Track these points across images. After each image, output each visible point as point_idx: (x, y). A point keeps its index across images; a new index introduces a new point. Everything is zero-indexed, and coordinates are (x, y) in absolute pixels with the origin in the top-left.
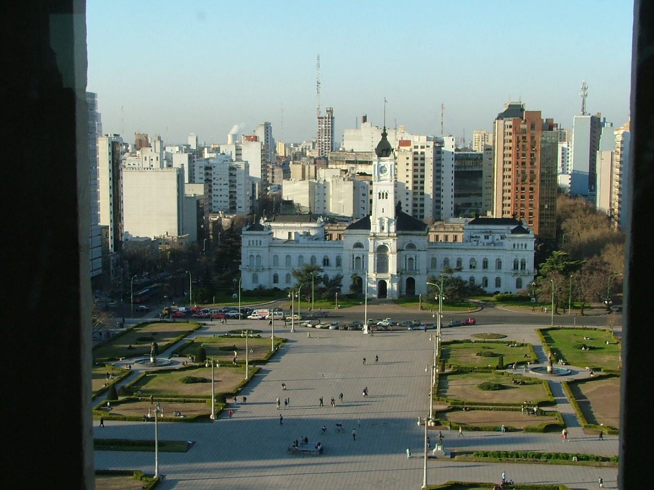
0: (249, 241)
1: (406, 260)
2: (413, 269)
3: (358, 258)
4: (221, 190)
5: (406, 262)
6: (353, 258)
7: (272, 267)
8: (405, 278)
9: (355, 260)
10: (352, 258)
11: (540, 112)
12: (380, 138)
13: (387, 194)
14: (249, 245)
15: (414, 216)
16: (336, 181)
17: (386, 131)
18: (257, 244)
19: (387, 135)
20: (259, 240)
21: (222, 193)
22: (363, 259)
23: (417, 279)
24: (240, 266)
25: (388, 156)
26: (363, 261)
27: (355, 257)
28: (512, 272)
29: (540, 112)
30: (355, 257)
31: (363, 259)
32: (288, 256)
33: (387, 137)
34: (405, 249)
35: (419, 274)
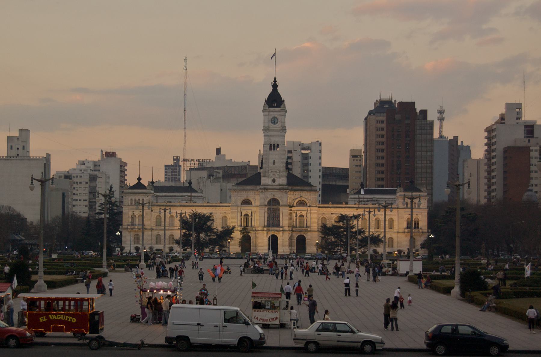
0: (131, 199)
1: (296, 217)
2: (304, 225)
3: (246, 215)
4: (81, 177)
5: (296, 219)
6: (241, 216)
7: (154, 228)
8: (296, 235)
9: (243, 217)
10: (239, 215)
11: (426, 110)
12: (270, 89)
13: (278, 145)
14: (131, 204)
15: (304, 177)
16: (203, 183)
17: (279, 89)
19: (277, 86)
21: (81, 180)
22: (252, 216)
23: (308, 236)
24: (121, 227)
26: (251, 219)
27: (243, 214)
28: (406, 230)
29: (426, 110)
30: (243, 214)
33: (278, 88)
34: (295, 205)
35: (310, 231)
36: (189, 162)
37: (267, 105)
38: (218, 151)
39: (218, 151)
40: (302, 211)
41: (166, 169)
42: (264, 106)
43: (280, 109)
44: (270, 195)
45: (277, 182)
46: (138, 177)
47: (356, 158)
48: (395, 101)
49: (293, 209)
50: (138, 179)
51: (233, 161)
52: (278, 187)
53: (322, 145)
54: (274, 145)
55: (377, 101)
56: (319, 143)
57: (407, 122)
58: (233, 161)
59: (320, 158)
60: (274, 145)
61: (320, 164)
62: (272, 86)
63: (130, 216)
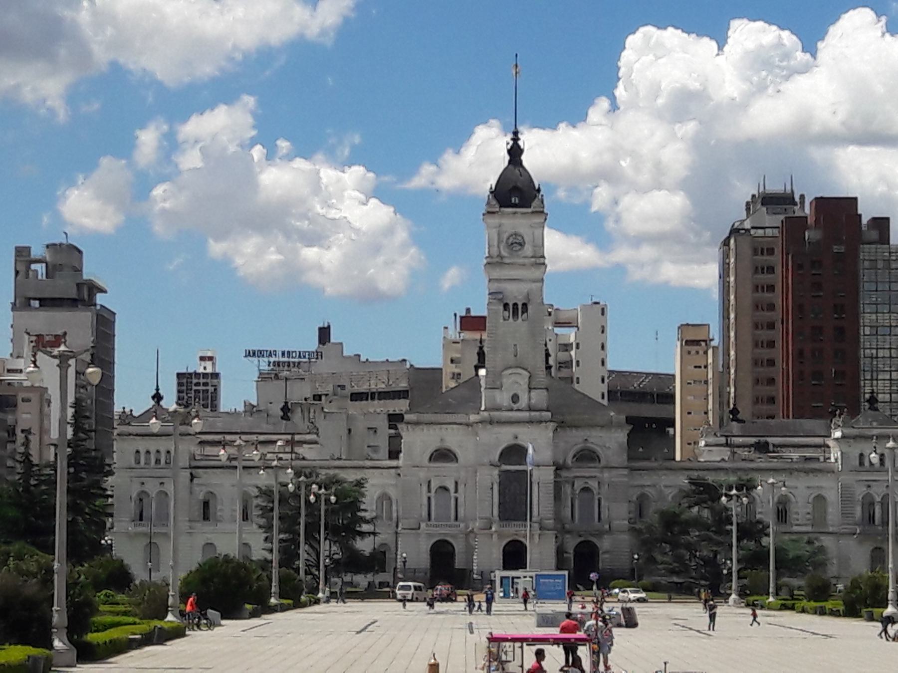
6: (429, 491)
8: (571, 543)
9: (432, 494)
10: (425, 488)
18: (147, 463)
20: (153, 450)
22: (456, 492)
25: (530, 207)
26: (456, 499)
31: (456, 492)
32: (820, 499)
33: (523, 157)
36: (266, 359)
37: (494, 202)
38: (324, 334)
39: (324, 334)
40: (583, 473)
41: (180, 384)
42: (488, 203)
43: (529, 210)
44: (505, 436)
45: (523, 402)
46: (154, 392)
47: (696, 348)
48: (802, 197)
49: (564, 474)
50: (153, 398)
51: (363, 359)
52: (525, 415)
53: (608, 312)
54: (515, 305)
55: (753, 196)
56: (598, 308)
57: (836, 249)
58: (363, 359)
59: (603, 347)
60: (515, 305)
61: (603, 363)
62: (509, 152)
63: (134, 496)
